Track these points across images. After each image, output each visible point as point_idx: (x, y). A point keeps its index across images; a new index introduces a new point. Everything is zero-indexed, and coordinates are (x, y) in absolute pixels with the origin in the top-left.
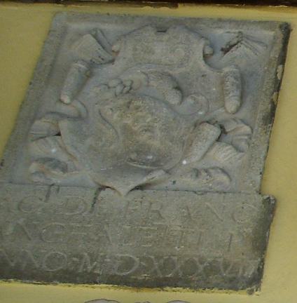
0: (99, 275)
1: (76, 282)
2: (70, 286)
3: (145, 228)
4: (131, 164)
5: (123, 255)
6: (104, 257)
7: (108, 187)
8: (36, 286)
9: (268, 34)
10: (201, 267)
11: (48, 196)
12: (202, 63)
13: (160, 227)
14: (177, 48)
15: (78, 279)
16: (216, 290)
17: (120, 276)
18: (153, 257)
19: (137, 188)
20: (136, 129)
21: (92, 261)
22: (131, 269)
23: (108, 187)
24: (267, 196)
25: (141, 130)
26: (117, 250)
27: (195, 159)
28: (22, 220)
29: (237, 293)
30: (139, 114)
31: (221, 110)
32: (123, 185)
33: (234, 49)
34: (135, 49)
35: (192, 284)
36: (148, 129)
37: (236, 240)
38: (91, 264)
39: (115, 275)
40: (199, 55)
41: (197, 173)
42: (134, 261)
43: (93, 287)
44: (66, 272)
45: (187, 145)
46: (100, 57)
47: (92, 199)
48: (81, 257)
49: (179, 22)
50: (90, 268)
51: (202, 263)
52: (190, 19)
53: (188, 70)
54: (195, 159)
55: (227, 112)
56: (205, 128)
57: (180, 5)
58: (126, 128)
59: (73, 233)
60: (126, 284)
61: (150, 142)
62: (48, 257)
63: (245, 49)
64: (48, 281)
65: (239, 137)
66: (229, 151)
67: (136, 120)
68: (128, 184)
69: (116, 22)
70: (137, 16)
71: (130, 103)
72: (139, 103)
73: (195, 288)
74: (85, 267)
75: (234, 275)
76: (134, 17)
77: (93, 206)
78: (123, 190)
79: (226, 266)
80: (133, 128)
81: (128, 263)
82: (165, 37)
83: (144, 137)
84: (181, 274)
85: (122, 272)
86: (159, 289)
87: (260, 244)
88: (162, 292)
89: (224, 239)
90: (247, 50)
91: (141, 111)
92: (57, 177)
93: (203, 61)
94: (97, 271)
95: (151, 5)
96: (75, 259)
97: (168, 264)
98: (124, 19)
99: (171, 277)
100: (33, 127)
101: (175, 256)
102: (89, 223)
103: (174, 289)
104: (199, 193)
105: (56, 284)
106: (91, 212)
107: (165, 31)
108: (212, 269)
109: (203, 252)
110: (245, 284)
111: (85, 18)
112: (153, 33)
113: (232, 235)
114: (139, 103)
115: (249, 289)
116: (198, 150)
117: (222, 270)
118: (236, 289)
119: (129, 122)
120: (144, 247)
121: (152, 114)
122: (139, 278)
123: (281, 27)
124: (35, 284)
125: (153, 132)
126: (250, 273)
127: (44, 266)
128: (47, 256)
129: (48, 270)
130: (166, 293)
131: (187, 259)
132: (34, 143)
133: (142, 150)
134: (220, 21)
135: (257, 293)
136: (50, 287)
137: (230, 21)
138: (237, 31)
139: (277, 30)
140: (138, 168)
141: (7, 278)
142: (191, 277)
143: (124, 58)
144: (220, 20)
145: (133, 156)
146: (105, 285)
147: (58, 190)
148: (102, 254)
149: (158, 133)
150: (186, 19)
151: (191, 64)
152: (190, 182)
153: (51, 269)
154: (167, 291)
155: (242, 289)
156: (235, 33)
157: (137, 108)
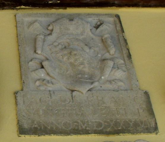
0: (89, 130)
1: (81, 134)
2: (78, 136)
3: (99, 108)
4: (81, 79)
5: (96, 120)
6: (88, 122)
7: (75, 90)
8: (64, 137)
9: (111, 19)
10: (131, 124)
11: (51, 96)
12: (90, 33)
13: (106, 107)
14: (79, 27)
15: (81, 132)
16: (142, 134)
17: (98, 130)
18: (109, 121)
19: (89, 90)
20: (76, 64)
21: (84, 125)
22: (102, 125)
23: (75, 90)
24: (145, 91)
25: (79, 64)
26: (93, 119)
27: (107, 76)
28: (44, 107)
29: (151, 134)
30: (77, 57)
31: (107, 54)
32: (84, 89)
33: (101, 26)
34: (60, 29)
35: (131, 132)
36: (82, 64)
37: (141, 111)
38: (84, 126)
39: (96, 130)
40: (89, 30)
41: (110, 82)
42: (101, 123)
43: (88, 136)
44: (74, 129)
45: (102, 70)
46: (43, 32)
47: (71, 96)
48: (78, 123)
49: (79, 15)
50: (84, 127)
51: (131, 122)
52: (76, 14)
53: (85, 37)
54: (107, 76)
55: (110, 55)
56: (108, 62)
57: (68, 8)
58: (71, 64)
59: (69, 112)
60: (117, 134)
61: (84, 69)
62: (64, 123)
63: (106, 26)
64: (68, 134)
65: (121, 65)
66: (121, 72)
67: (76, 60)
68: (86, 89)
69: (44, 17)
70: (53, 14)
71: (71, 52)
72: (75, 52)
73: (133, 133)
74: (81, 127)
75: (147, 127)
76: (51, 14)
77: (72, 99)
78: (84, 91)
79: (142, 123)
80: (75, 63)
81: (100, 124)
82: (74, 22)
83: (81, 68)
84: (124, 127)
85: (99, 128)
86: (117, 135)
87: (151, 112)
88: (118, 136)
89: (134, 112)
90: (107, 27)
91: (77, 56)
92: (50, 87)
93: (54, 29)
94: (88, 129)
95: (62, 8)
96: (75, 124)
97: (116, 123)
98: (47, 15)
99: (120, 129)
100: (29, 65)
101: (118, 120)
102: (74, 107)
103: (124, 134)
104: (116, 91)
105: (72, 135)
106: (73, 102)
107: (73, 20)
108: (136, 125)
109: (129, 117)
110: (153, 130)
111: (29, 15)
112: (68, 21)
113: (138, 109)
114: (75, 52)
115: (156, 132)
116: (108, 71)
117: (141, 125)
118: (151, 133)
119: (72, 60)
120: (103, 117)
121: (82, 57)
122: (107, 130)
123: (116, 16)
124: (62, 136)
125: (84, 65)
126: (153, 125)
127: (64, 128)
128: (63, 123)
129: (66, 129)
130: (120, 136)
131: (124, 120)
132: (33, 72)
133: (82, 73)
134: (89, 15)
135: (159, 134)
136: (69, 137)
137: (94, 14)
138: (98, 19)
139: (115, 17)
140: (87, 81)
141: (50, 134)
142: (129, 128)
143: (56, 33)
144: (89, 14)
145: (80, 76)
146: (94, 135)
147: (54, 93)
148: (86, 121)
149: (87, 65)
150: (74, 14)
151: (86, 34)
152: (108, 86)
153: (67, 128)
154: (120, 135)
155: (153, 132)
156: (97, 19)
157: (75, 55)
